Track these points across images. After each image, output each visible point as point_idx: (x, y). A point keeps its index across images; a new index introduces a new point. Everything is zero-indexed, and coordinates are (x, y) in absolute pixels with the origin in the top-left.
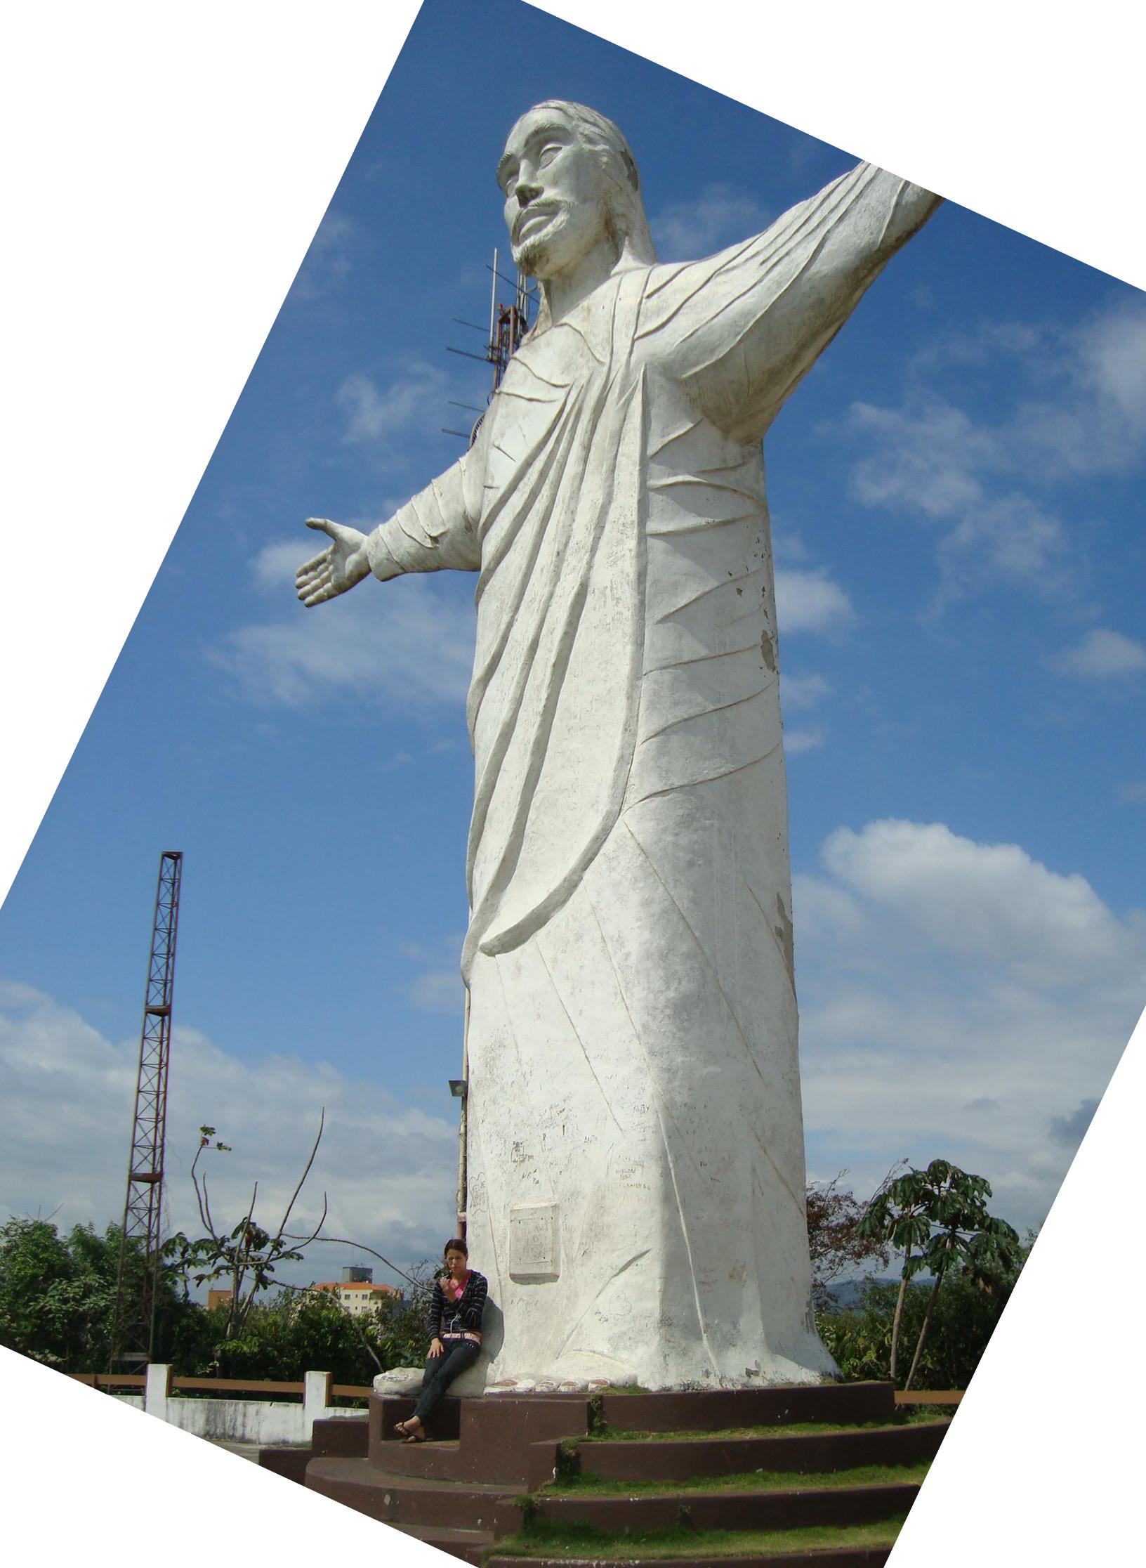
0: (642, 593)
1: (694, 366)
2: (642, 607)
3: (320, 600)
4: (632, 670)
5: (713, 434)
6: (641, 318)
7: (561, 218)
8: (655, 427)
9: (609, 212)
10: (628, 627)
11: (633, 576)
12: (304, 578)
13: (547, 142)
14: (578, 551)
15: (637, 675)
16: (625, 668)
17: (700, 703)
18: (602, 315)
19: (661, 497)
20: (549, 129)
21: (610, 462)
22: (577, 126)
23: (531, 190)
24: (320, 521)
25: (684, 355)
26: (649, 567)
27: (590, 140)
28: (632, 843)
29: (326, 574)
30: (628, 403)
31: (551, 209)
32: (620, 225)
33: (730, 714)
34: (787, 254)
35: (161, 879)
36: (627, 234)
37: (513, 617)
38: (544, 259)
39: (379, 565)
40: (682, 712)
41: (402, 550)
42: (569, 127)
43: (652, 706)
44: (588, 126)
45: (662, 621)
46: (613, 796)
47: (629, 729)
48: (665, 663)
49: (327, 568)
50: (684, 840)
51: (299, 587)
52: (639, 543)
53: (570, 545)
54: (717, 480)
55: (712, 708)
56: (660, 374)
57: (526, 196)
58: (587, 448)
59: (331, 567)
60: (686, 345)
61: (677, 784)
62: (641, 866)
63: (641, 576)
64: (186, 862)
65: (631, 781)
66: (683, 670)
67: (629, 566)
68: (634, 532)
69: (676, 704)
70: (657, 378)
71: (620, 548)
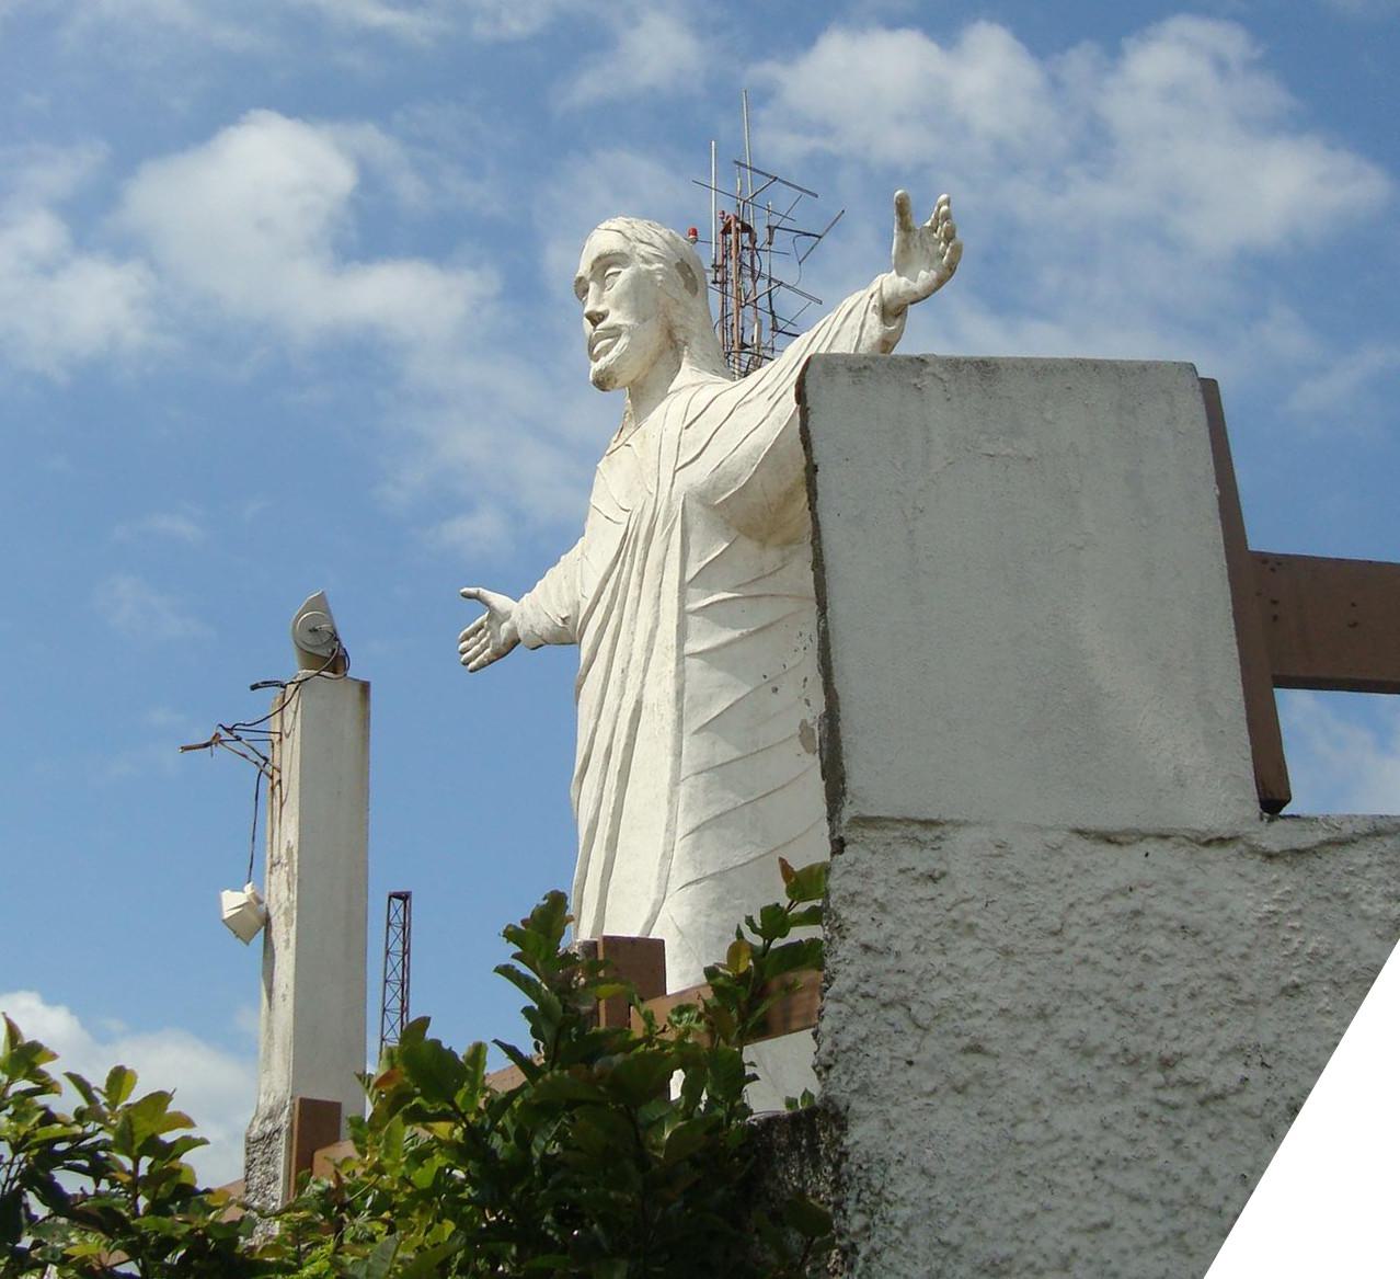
0: (680, 710)
1: (723, 493)
2: (680, 721)
3: (482, 666)
4: (671, 778)
5: (749, 546)
6: (681, 449)
7: (623, 341)
8: (693, 553)
9: (669, 322)
10: (669, 741)
11: (672, 695)
12: (465, 643)
13: (609, 266)
14: (636, 668)
15: (675, 782)
16: (667, 776)
17: (732, 799)
18: (653, 443)
19: (697, 619)
20: (609, 255)
21: (655, 590)
22: (635, 247)
23: (598, 314)
24: (472, 590)
25: (714, 487)
26: (687, 685)
27: (647, 261)
28: (673, 926)
29: (484, 640)
30: (670, 532)
31: (615, 333)
32: (680, 336)
33: (760, 804)
34: (785, 393)
35: (389, 924)
36: (686, 344)
37: (596, 723)
38: (613, 381)
39: (526, 636)
40: (715, 810)
41: (541, 626)
42: (626, 250)
43: (688, 808)
44: (643, 246)
45: (695, 733)
46: (659, 886)
47: (670, 829)
48: (699, 769)
49: (485, 633)
50: (716, 919)
51: (463, 653)
52: (677, 665)
53: (632, 662)
54: (755, 591)
55: (743, 802)
56: (697, 502)
57: (596, 319)
58: (642, 575)
59: (488, 634)
60: (715, 475)
61: (709, 873)
62: (680, 945)
63: (680, 693)
64: (414, 901)
65: (672, 873)
66: (718, 773)
67: (669, 686)
68: (673, 655)
69: (709, 803)
70: (695, 505)
71: (663, 669)
